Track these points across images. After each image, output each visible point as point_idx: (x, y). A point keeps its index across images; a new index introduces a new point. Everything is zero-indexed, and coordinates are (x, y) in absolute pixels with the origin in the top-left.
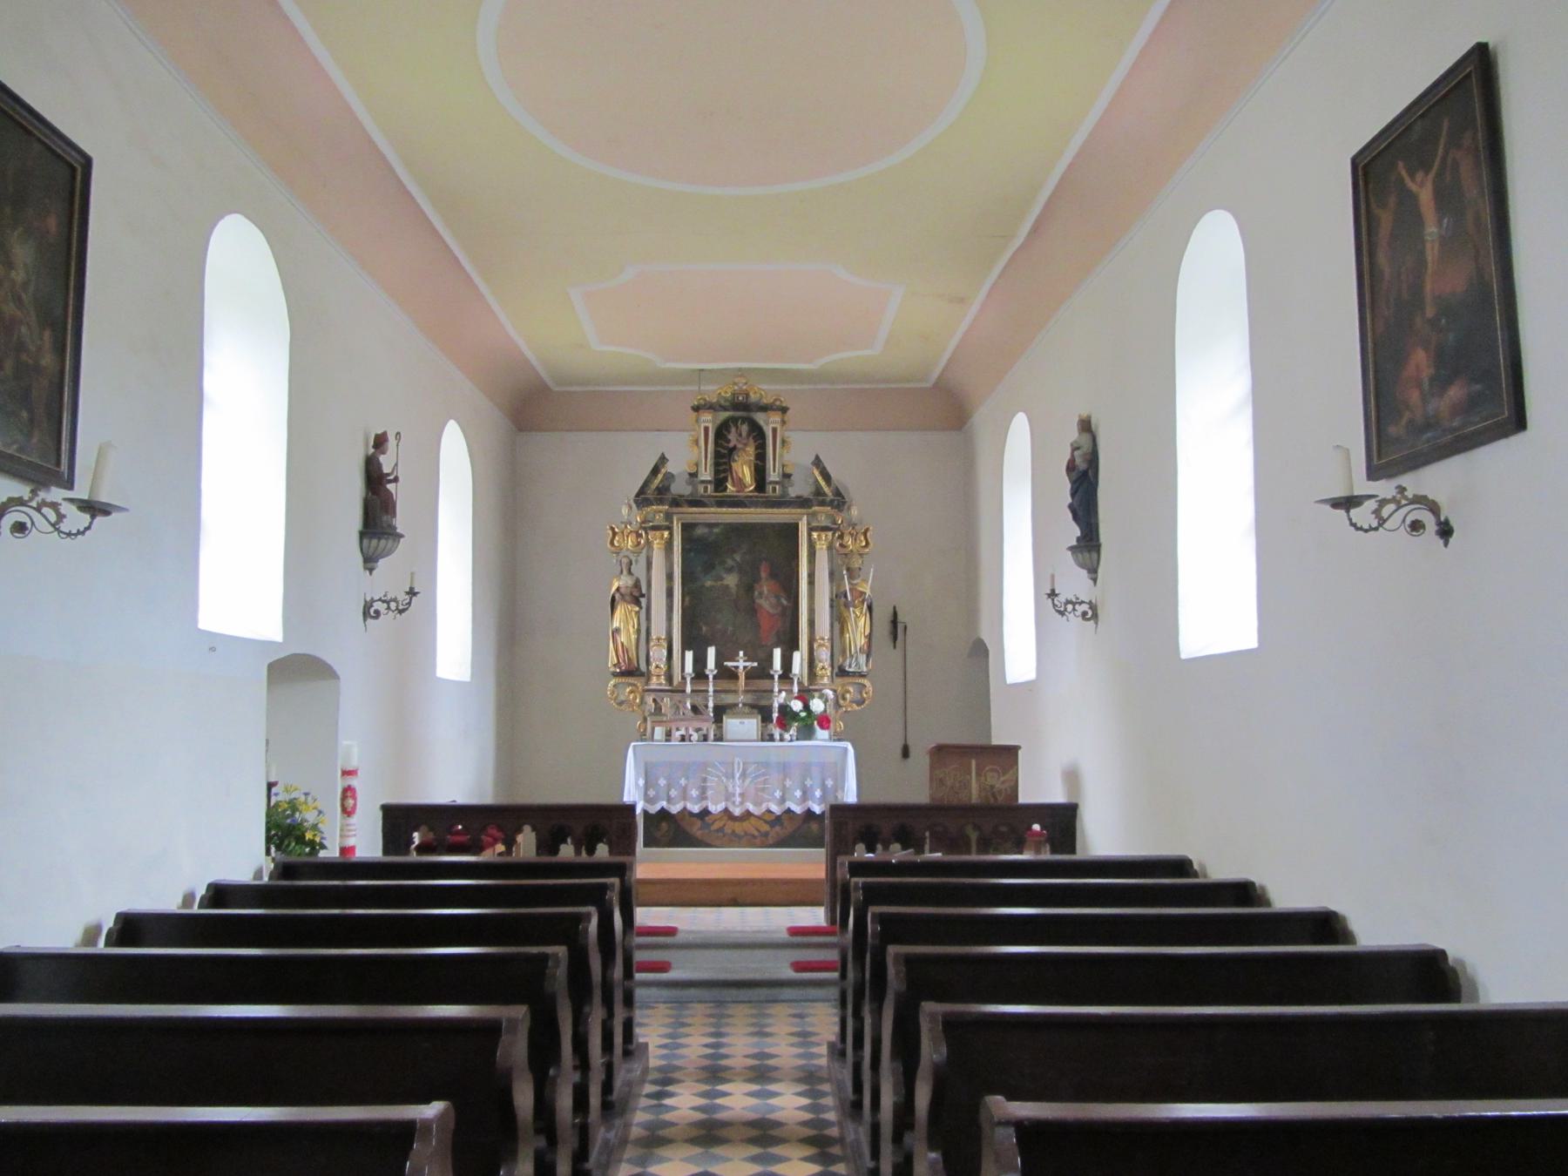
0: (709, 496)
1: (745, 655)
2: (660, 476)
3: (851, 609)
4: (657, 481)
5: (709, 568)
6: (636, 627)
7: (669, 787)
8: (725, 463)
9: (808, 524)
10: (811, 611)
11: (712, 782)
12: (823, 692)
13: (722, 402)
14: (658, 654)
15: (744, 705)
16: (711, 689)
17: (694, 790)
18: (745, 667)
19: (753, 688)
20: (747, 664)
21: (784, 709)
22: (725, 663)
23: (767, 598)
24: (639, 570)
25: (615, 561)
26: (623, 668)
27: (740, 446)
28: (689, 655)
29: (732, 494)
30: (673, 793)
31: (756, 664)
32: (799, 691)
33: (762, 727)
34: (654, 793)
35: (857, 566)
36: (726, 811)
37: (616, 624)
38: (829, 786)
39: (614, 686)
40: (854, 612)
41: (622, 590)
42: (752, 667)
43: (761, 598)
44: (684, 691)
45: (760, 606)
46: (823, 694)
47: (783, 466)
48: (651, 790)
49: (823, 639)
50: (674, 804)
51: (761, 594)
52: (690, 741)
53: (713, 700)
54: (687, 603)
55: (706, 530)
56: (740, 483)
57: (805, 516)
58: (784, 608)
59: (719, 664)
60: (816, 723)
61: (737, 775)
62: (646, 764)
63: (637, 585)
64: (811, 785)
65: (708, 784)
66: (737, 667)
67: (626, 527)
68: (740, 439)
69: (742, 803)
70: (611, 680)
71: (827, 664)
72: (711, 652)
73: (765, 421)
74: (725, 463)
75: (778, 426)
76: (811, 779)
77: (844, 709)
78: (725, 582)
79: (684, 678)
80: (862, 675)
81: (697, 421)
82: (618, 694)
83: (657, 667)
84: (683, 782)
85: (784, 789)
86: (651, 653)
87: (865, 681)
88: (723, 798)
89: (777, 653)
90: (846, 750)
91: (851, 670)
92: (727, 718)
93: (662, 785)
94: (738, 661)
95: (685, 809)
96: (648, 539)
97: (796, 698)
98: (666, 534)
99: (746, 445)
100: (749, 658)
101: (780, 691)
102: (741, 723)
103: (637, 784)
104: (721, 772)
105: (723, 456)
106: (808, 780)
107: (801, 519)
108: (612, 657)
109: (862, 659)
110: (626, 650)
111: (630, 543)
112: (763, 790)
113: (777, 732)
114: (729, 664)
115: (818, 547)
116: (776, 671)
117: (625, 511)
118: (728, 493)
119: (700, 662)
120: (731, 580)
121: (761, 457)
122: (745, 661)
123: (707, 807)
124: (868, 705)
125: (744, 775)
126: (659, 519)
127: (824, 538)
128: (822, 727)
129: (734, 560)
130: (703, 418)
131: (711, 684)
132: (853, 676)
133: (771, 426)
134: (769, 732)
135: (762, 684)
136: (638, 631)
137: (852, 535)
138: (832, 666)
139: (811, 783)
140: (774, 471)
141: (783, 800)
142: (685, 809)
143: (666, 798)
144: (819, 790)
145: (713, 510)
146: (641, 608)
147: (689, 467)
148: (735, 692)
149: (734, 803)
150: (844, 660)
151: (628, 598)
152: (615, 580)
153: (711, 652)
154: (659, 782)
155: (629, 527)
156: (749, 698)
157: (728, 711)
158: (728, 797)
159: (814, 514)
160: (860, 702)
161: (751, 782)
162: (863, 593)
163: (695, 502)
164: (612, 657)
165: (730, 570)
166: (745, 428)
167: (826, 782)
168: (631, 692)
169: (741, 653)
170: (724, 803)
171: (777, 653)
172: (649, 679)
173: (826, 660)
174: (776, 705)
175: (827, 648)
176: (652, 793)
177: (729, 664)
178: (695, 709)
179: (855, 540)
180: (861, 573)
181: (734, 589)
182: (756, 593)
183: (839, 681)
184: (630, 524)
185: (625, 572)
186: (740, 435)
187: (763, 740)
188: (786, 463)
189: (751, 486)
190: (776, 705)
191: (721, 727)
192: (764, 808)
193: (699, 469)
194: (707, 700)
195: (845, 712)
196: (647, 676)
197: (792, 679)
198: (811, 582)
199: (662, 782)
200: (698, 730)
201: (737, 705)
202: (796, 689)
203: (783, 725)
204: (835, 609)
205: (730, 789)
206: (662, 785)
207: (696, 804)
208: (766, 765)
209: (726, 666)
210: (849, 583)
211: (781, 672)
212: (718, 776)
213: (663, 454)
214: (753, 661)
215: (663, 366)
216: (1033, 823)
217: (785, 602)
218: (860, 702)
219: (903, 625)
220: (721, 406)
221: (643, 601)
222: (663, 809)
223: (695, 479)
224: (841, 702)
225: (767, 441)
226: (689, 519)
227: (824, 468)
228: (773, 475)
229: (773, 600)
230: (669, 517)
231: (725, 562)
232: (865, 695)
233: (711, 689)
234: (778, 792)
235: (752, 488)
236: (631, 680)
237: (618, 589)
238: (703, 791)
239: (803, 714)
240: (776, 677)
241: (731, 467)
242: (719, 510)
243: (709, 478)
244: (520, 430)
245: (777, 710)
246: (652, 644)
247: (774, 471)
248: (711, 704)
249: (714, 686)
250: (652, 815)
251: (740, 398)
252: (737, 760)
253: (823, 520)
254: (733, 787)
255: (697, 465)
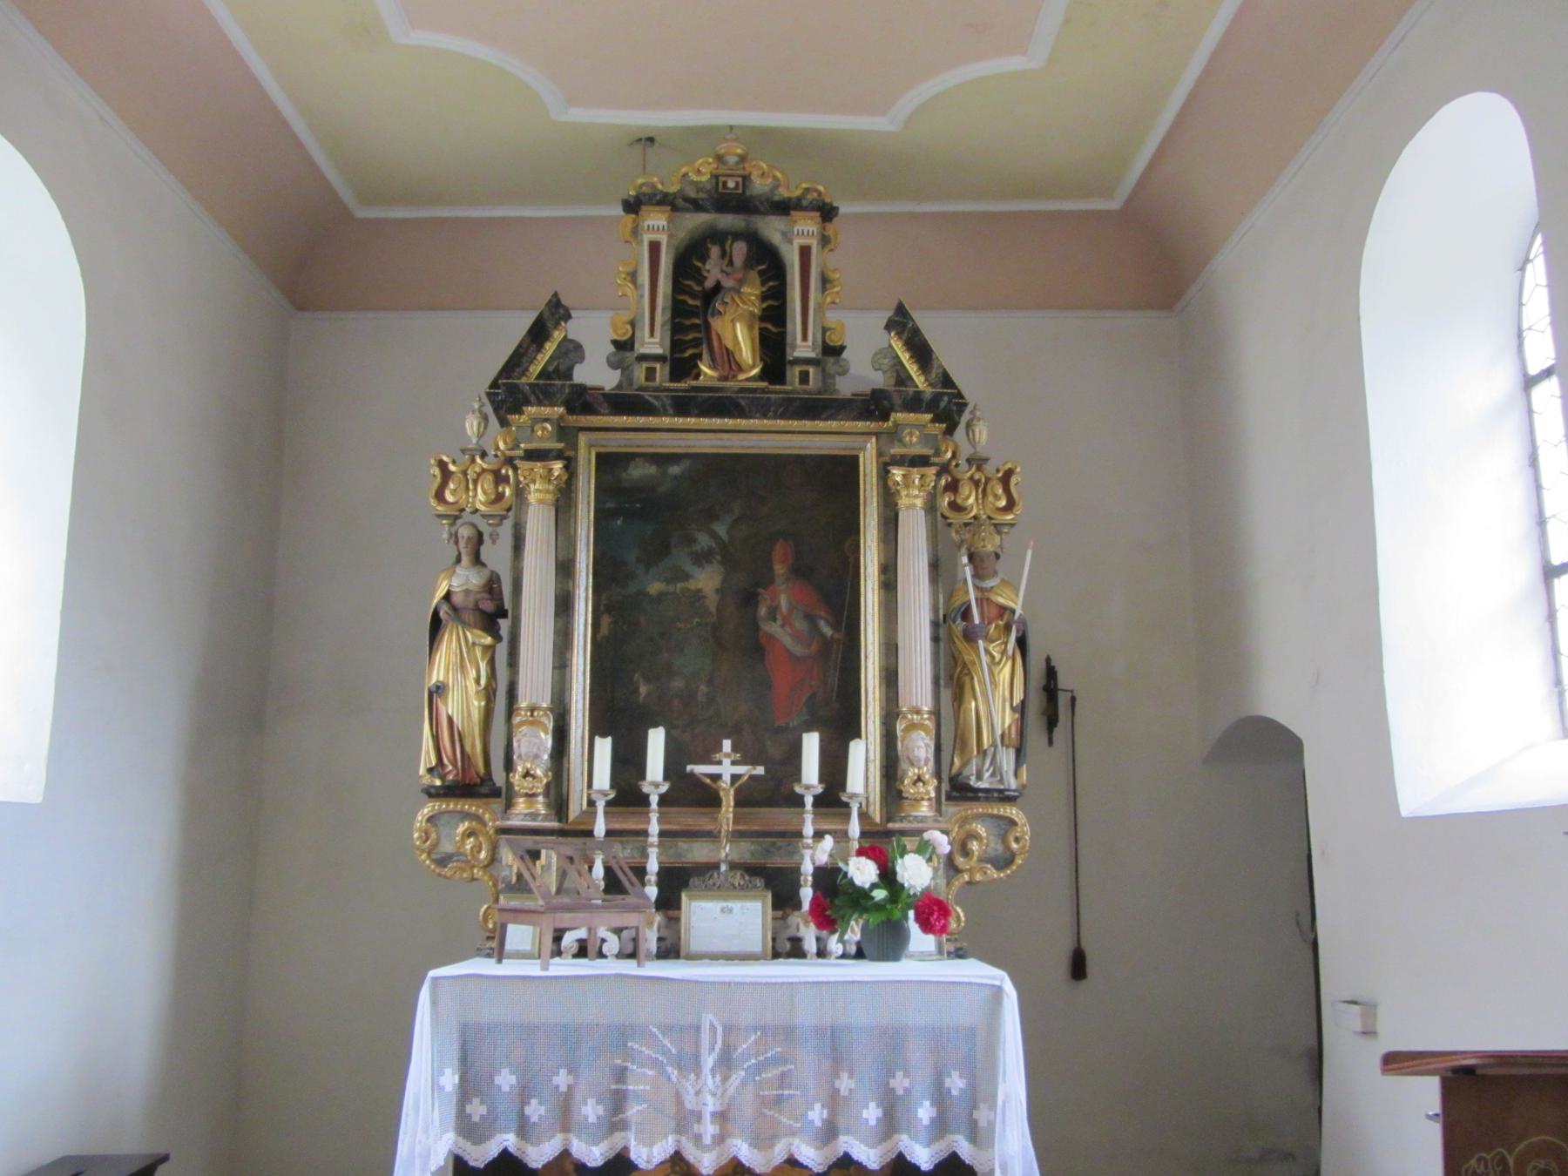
0: (657, 389)
1: (735, 749)
2: (550, 348)
3: (981, 642)
4: (542, 359)
5: (657, 552)
6: (483, 681)
7: (524, 1093)
8: (695, 327)
9: (880, 454)
10: (890, 649)
11: (640, 1082)
12: (926, 836)
13: (692, 194)
14: (534, 744)
15: (733, 866)
16: (654, 828)
17: (591, 1101)
18: (735, 778)
19: (756, 828)
20: (741, 770)
21: (830, 880)
22: (689, 768)
23: (786, 622)
24: (497, 556)
25: (445, 536)
26: (451, 777)
27: (727, 283)
28: (604, 747)
29: (709, 384)
30: (535, 1110)
31: (760, 770)
32: (863, 834)
33: (774, 919)
34: (483, 1110)
35: (990, 548)
36: (677, 1158)
37: (437, 675)
38: (955, 1092)
39: (430, 819)
40: (987, 651)
41: (457, 599)
42: (752, 778)
43: (775, 620)
44: (589, 833)
45: (771, 637)
46: (927, 842)
47: (825, 330)
48: (476, 1101)
49: (918, 712)
50: (537, 1143)
51: (773, 614)
52: (601, 955)
53: (660, 855)
54: (605, 630)
55: (652, 470)
56: (728, 361)
57: (874, 439)
58: (826, 644)
59: (673, 769)
60: (911, 914)
61: (709, 1061)
62: (464, 1029)
63: (492, 586)
64: (908, 1091)
65: (631, 1087)
66: (716, 778)
67: (473, 461)
68: (729, 269)
69: (720, 1139)
70: (422, 806)
71: (927, 771)
72: (656, 740)
73: (784, 234)
74: (695, 327)
75: (814, 243)
76: (906, 1075)
77: (966, 877)
78: (692, 585)
79: (591, 803)
80: (1005, 797)
81: (635, 232)
82: (438, 839)
83: (527, 774)
84: (562, 1079)
85: (834, 1101)
86: (515, 745)
87: (1012, 811)
88: (672, 1124)
89: (811, 744)
90: (997, 992)
91: (983, 785)
92: (691, 898)
93: (506, 1088)
94: (720, 763)
95: (565, 1154)
96: (518, 482)
97: (861, 852)
98: (557, 466)
99: (741, 282)
100: (746, 755)
101: (818, 835)
102: (723, 910)
103: (436, 1087)
104: (666, 1052)
105: (692, 312)
106: (899, 1074)
107: (863, 449)
108: (428, 752)
109: (1007, 759)
110: (457, 736)
111: (481, 497)
112: (779, 1100)
113: (809, 935)
114: (700, 769)
115: (903, 502)
116: (808, 787)
117: (472, 425)
118: (702, 381)
119: (629, 762)
120: (707, 580)
121: (773, 315)
122: (734, 763)
123: (626, 1149)
124: (1020, 867)
125: (726, 1063)
126: (544, 436)
127: (917, 481)
128: (926, 927)
129: (714, 535)
130: (650, 222)
131: (654, 817)
132: (987, 799)
133: (798, 242)
134: (791, 932)
135: (777, 817)
136: (489, 694)
137: (977, 483)
138: (938, 774)
139: (906, 1082)
140: (805, 338)
141: (830, 1132)
142: (565, 1154)
143: (514, 1126)
144: (927, 1103)
145: (666, 421)
146: (497, 637)
147: (615, 328)
148: (712, 836)
149: (698, 1139)
150: (965, 764)
151: (468, 616)
152: (442, 576)
153: (656, 740)
154: (498, 1080)
155: (478, 460)
156: (744, 851)
157: (694, 881)
158: (685, 1121)
159: (894, 435)
160: (1004, 861)
161: (744, 1083)
162: (1003, 610)
163: (622, 402)
164: (428, 752)
165: (702, 559)
166: (739, 250)
167: (948, 1082)
168: (470, 833)
169: (727, 745)
170: (670, 1138)
171: (811, 744)
172: (509, 805)
173: (927, 760)
174: (807, 868)
175: (927, 733)
176: (477, 1110)
177: (700, 769)
178: (613, 885)
179: (984, 491)
180: (1000, 565)
181: (712, 602)
182: (763, 611)
183: (951, 809)
184: (484, 455)
185: (465, 559)
186: (731, 263)
187: (776, 955)
188: (828, 324)
189: (753, 366)
190: (807, 868)
191: (677, 920)
192: (779, 1153)
193: (638, 334)
194: (645, 856)
195: (969, 883)
196: (506, 796)
197: (847, 805)
198: (889, 584)
199: (506, 1080)
200: (618, 931)
201: (716, 866)
202: (854, 828)
203: (826, 919)
204: (942, 645)
205: (690, 1102)
206: (506, 1088)
207: (596, 1144)
208: (789, 1033)
209: (692, 774)
210: (976, 587)
211: (819, 790)
212: (655, 1064)
213: (556, 295)
214: (754, 762)
215: (563, 118)
216: (685, 768)
217: (828, 631)
218: (1004, 861)
219: (1069, 695)
220: (687, 200)
221: (504, 625)
222: (505, 1153)
223: (628, 354)
224: (960, 861)
225: (789, 278)
226: (615, 443)
227: (916, 331)
228: (802, 348)
229: (800, 625)
230: (565, 433)
231: (691, 540)
232: (1014, 846)
233: (654, 828)
234: (818, 1106)
235: (755, 372)
236: (468, 806)
237: (448, 597)
238: (617, 1102)
239: (880, 894)
240: (809, 800)
241: (708, 327)
242: (680, 421)
243: (659, 351)
244: (301, 308)
245: (810, 878)
246: (516, 720)
247: (805, 338)
248: (653, 866)
249: (660, 821)
250: (474, 1169)
251: (731, 184)
252: (708, 1018)
253: (913, 444)
254: (698, 1093)
255: (633, 324)
